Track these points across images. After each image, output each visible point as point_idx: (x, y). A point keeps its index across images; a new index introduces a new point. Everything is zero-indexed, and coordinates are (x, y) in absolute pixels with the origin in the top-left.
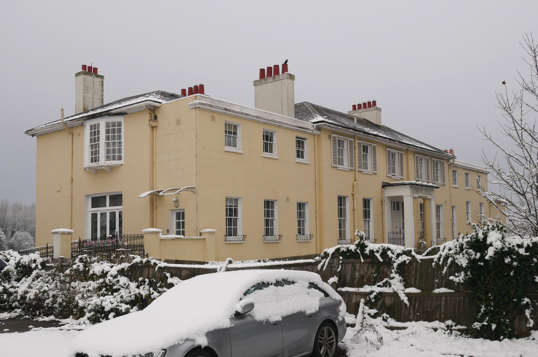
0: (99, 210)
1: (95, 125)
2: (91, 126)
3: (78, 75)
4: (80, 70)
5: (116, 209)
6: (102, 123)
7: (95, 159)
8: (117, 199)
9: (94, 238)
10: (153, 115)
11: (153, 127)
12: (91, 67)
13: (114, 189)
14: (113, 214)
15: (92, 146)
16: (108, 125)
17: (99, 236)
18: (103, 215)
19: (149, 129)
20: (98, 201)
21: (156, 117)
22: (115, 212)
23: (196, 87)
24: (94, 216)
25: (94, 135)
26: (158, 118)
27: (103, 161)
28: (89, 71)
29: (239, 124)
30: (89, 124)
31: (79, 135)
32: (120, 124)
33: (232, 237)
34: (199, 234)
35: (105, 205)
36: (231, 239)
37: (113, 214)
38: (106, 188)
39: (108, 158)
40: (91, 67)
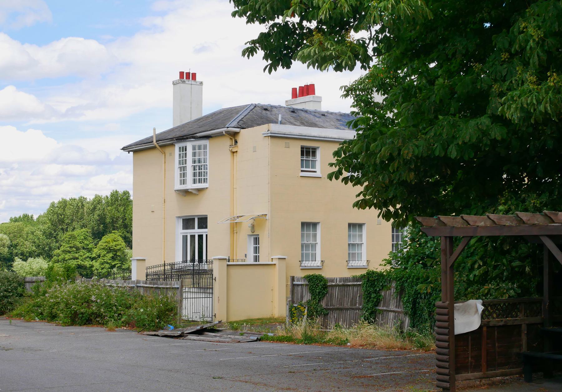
0: (189, 232)
1: (183, 147)
2: (180, 148)
3: (174, 84)
4: (177, 77)
5: (202, 231)
6: (189, 145)
7: (183, 182)
8: (203, 222)
9: (185, 261)
10: (233, 140)
11: (234, 152)
12: (189, 73)
13: (201, 212)
14: (200, 237)
15: (180, 168)
16: (194, 148)
17: (189, 259)
18: (193, 237)
19: (229, 154)
20: (188, 223)
21: (236, 142)
22: (202, 235)
23: (307, 86)
24: (185, 238)
25: (183, 158)
26: (238, 144)
27: (190, 185)
28: (187, 77)
29: (318, 147)
30: (177, 146)
31: (171, 154)
32: (205, 147)
33: (310, 262)
34: (270, 260)
35: (194, 228)
36: (306, 265)
37: (200, 237)
38: (196, 210)
39: (194, 182)
40: (189, 73)
